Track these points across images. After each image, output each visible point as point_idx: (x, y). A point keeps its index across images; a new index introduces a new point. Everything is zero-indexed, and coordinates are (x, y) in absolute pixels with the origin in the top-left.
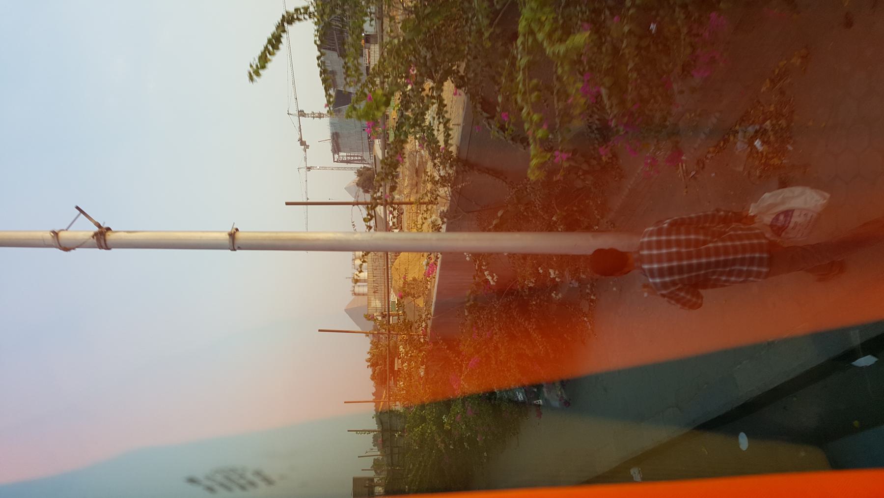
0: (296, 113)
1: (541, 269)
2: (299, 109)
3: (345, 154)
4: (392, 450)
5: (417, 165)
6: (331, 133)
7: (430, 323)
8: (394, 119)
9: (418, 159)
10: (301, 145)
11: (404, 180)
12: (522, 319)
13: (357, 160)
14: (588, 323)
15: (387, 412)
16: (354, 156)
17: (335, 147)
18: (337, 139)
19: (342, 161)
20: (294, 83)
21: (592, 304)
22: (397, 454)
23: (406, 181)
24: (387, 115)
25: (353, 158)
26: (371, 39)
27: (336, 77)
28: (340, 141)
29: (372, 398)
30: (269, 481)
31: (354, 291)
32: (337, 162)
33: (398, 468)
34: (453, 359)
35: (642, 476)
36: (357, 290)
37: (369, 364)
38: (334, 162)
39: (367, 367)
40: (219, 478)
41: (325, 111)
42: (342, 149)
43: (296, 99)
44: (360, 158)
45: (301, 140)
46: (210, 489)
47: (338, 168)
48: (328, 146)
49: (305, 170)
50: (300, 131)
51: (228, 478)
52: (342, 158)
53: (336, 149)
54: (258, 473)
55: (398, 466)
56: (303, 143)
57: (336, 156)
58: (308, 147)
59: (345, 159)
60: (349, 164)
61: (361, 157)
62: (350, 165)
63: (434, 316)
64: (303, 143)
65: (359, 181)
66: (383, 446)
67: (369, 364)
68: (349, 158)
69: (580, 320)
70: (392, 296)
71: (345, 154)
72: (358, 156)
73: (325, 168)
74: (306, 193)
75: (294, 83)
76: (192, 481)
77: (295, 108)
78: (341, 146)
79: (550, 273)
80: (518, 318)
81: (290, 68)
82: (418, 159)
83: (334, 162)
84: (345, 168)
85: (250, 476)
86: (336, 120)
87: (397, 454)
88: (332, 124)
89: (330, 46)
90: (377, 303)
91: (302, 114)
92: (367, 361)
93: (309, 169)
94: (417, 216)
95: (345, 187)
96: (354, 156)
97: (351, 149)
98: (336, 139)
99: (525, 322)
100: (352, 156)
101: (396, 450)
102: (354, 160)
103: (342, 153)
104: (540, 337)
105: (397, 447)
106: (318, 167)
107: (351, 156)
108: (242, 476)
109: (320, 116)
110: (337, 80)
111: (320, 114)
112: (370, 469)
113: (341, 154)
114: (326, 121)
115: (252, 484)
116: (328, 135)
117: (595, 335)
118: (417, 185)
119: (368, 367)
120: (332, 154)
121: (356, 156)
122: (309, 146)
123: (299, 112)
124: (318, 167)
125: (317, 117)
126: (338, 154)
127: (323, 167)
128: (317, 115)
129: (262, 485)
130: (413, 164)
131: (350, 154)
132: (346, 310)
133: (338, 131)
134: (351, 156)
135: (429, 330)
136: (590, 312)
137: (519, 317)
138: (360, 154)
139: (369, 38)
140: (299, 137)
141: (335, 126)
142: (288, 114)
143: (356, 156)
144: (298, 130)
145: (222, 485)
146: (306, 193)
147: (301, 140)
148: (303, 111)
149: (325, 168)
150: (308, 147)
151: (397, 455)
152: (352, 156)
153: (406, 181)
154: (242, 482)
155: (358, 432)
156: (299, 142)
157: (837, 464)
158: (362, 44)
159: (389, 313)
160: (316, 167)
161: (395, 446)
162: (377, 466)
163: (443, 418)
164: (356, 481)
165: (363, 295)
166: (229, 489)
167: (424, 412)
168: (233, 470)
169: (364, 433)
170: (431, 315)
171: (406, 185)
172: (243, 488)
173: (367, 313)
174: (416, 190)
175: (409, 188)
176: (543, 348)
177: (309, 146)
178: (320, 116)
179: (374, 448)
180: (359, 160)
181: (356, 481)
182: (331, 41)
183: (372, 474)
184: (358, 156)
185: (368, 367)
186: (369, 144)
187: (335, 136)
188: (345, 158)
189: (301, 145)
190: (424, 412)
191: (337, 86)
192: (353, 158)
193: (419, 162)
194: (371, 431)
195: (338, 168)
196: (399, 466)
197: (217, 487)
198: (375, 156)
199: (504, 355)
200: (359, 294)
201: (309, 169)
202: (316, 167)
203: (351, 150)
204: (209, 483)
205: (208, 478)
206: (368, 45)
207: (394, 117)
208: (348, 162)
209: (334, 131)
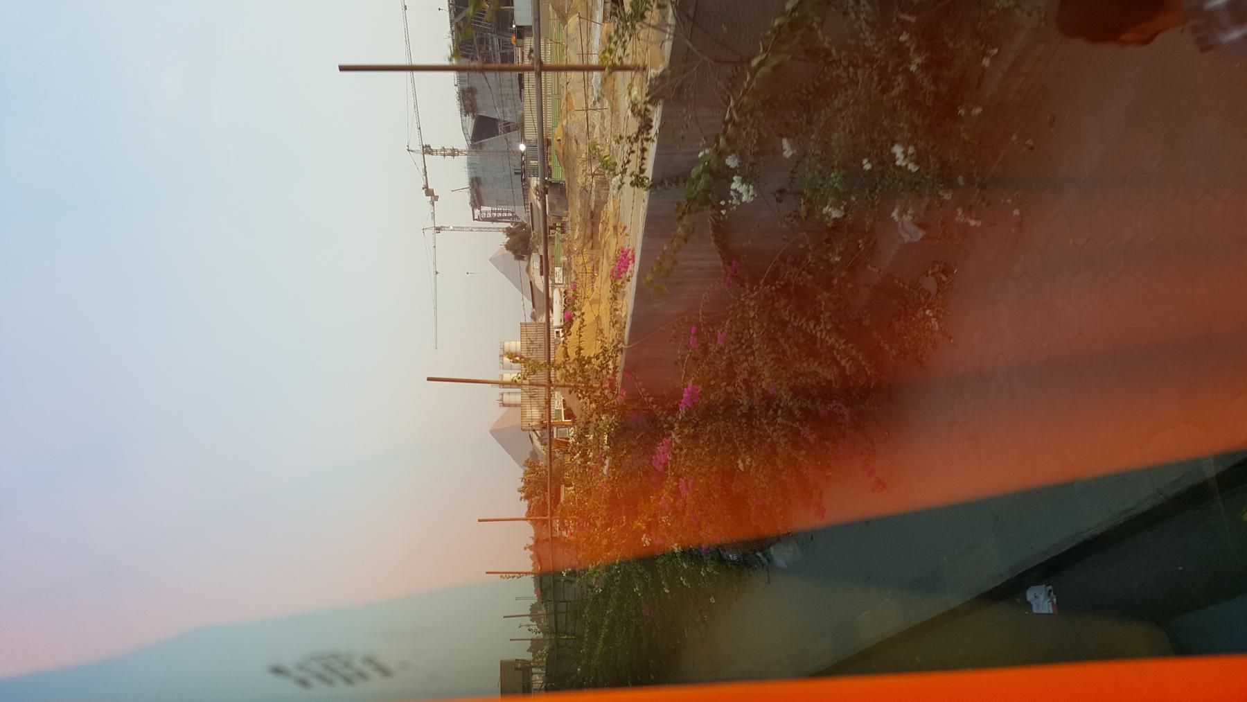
0: (420, 148)
1: (869, 162)
2: (424, 144)
3: (490, 209)
4: (556, 608)
5: (593, 206)
6: (469, 178)
7: (620, 359)
8: (559, 140)
9: (593, 198)
10: (427, 195)
11: (573, 230)
12: (800, 320)
13: (507, 217)
14: (933, 320)
15: (547, 540)
16: (502, 212)
17: (476, 199)
18: (478, 187)
19: (486, 219)
20: (416, 106)
21: (944, 278)
22: (563, 613)
23: (577, 231)
24: (548, 140)
25: (500, 215)
26: (525, 31)
27: (476, 96)
28: (482, 189)
29: (522, 508)
30: (384, 671)
31: (502, 400)
32: (478, 220)
33: (565, 637)
34: (663, 419)
35: (1055, 600)
36: (507, 399)
37: (523, 495)
38: (474, 220)
39: (519, 498)
40: (316, 666)
41: (462, 143)
42: (485, 202)
43: (420, 128)
44: (511, 215)
45: (426, 187)
46: (303, 683)
47: (480, 229)
48: (466, 197)
49: (432, 231)
50: (426, 175)
51: (327, 667)
52: (485, 214)
53: (477, 202)
54: (370, 660)
55: (566, 633)
56: (429, 192)
57: (477, 211)
58: (436, 198)
59: (489, 215)
60: (495, 223)
61: (513, 213)
62: (496, 225)
63: (628, 345)
64: (429, 192)
65: (508, 242)
66: (542, 599)
67: (523, 495)
68: (495, 214)
69: (914, 319)
70: (556, 402)
71: (489, 209)
72: (507, 212)
73: (461, 229)
74: (435, 264)
75: (416, 106)
76: (278, 671)
77: (418, 142)
78: (484, 197)
79: (894, 155)
80: (792, 319)
81: (410, 84)
82: (593, 198)
83: (474, 220)
84: (489, 229)
85: (359, 665)
86: (477, 159)
87: (563, 613)
88: (471, 165)
89: (467, 52)
90: (535, 413)
91: (427, 150)
92: (519, 491)
93: (438, 229)
94: (593, 283)
95: (489, 257)
96: (502, 212)
97: (497, 201)
98: (476, 186)
99: (807, 324)
100: (499, 212)
101: (563, 607)
102: (502, 218)
103: (485, 207)
104: (842, 341)
105: (564, 601)
106: (451, 228)
107: (497, 212)
108: (347, 665)
109: (454, 153)
110: (477, 101)
111: (453, 150)
112: (446, 63)
113: (484, 208)
114: (462, 160)
115: (362, 675)
116: (465, 181)
117: (950, 338)
118: (592, 237)
119: (521, 500)
120: (530, 638)
121: (505, 212)
122: (438, 197)
123: (423, 147)
124: (451, 228)
125: (449, 155)
126: (480, 209)
127: (458, 227)
128: (449, 152)
129: (375, 676)
130: (586, 205)
131: (496, 209)
132: (494, 433)
133: (480, 175)
134: (497, 212)
135: (619, 377)
136: (940, 297)
137: (795, 318)
138: (511, 208)
139: (523, 31)
140: (423, 183)
141: (473, 168)
142: (408, 150)
143: (505, 212)
144: (422, 173)
145: (320, 677)
146: (435, 264)
147: (426, 187)
148: (429, 146)
149: (461, 229)
150: (436, 198)
151: (565, 614)
152: (499, 212)
153: (577, 231)
154: (348, 672)
155: (504, 575)
156: (424, 191)
157: (1182, 648)
158: (513, 42)
159: (550, 422)
160: (449, 227)
161: (562, 600)
162: (535, 645)
163: (643, 539)
164: (505, 666)
165: (516, 406)
166: (329, 682)
167: (609, 529)
168: (335, 656)
169: (513, 577)
170: (623, 343)
171: (576, 237)
172: (348, 681)
173: (527, 523)
174: (591, 245)
175: (580, 241)
176: (847, 362)
177: (438, 197)
178: (454, 153)
179: (532, 623)
180: (509, 218)
181: (505, 666)
182: (468, 45)
183: (529, 657)
184: (507, 212)
185: (521, 500)
186: (523, 189)
187: (475, 183)
188: (490, 214)
189: (427, 195)
190: (609, 529)
191: (477, 109)
192: (500, 215)
193: (596, 202)
194: (522, 573)
195: (480, 229)
196: (567, 634)
197: (313, 681)
198: (531, 204)
199: (768, 380)
200: (509, 405)
201: (438, 229)
202: (449, 227)
203: (498, 203)
204: (301, 674)
205: (300, 667)
206: (520, 41)
207: (558, 138)
208: (493, 220)
209: (466, 86)
